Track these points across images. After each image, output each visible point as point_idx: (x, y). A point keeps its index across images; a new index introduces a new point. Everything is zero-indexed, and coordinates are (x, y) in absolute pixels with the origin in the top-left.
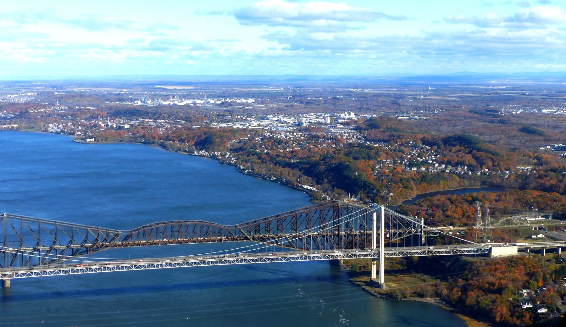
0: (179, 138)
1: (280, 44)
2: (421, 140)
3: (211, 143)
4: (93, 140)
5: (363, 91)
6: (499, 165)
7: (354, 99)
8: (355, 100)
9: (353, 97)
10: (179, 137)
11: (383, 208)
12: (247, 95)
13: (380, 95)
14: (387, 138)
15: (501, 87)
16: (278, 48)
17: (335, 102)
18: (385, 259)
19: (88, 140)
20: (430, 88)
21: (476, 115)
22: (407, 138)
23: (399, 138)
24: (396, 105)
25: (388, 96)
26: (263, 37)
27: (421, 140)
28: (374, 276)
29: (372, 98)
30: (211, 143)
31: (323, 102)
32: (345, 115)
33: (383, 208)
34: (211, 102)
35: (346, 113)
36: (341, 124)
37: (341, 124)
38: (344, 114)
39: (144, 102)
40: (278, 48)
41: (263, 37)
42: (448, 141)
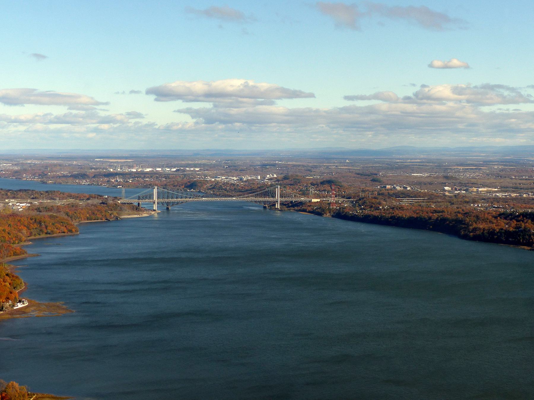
0: (173, 185)
1: (192, 119)
2: (310, 183)
3: (196, 186)
4: (121, 186)
5: (287, 163)
6: (341, 190)
7: (278, 168)
8: (279, 169)
9: (277, 167)
10: (173, 184)
11: (279, 186)
12: (195, 166)
13: (299, 166)
14: (293, 183)
15: (418, 161)
16: (189, 121)
17: (263, 169)
18: (280, 201)
19: (118, 187)
20: (348, 160)
21: (358, 176)
22: (303, 183)
23: (299, 183)
24: (308, 171)
25: (303, 166)
26: (175, 111)
27: (310, 183)
28: (277, 207)
29: (292, 168)
30: (196, 186)
31: (253, 170)
32: (270, 176)
33: (279, 186)
34: (167, 170)
35: (271, 175)
36: (267, 179)
37: (267, 179)
38: (269, 175)
39: (115, 170)
40: (189, 121)
41: (175, 111)
42: (322, 183)
